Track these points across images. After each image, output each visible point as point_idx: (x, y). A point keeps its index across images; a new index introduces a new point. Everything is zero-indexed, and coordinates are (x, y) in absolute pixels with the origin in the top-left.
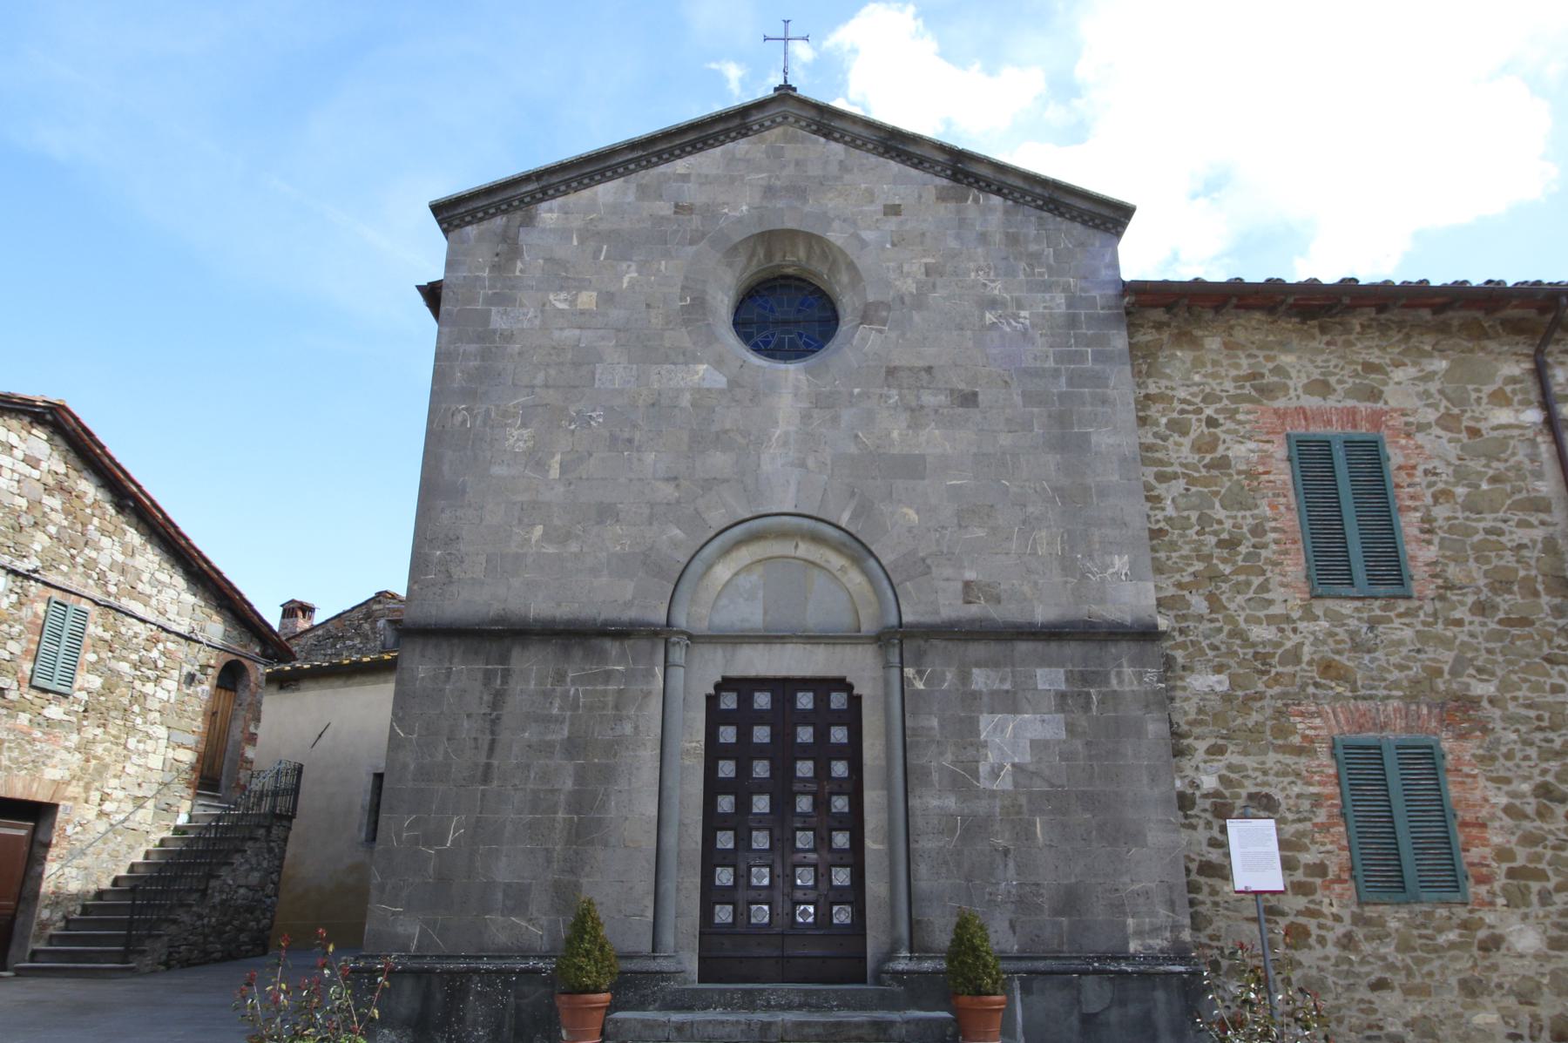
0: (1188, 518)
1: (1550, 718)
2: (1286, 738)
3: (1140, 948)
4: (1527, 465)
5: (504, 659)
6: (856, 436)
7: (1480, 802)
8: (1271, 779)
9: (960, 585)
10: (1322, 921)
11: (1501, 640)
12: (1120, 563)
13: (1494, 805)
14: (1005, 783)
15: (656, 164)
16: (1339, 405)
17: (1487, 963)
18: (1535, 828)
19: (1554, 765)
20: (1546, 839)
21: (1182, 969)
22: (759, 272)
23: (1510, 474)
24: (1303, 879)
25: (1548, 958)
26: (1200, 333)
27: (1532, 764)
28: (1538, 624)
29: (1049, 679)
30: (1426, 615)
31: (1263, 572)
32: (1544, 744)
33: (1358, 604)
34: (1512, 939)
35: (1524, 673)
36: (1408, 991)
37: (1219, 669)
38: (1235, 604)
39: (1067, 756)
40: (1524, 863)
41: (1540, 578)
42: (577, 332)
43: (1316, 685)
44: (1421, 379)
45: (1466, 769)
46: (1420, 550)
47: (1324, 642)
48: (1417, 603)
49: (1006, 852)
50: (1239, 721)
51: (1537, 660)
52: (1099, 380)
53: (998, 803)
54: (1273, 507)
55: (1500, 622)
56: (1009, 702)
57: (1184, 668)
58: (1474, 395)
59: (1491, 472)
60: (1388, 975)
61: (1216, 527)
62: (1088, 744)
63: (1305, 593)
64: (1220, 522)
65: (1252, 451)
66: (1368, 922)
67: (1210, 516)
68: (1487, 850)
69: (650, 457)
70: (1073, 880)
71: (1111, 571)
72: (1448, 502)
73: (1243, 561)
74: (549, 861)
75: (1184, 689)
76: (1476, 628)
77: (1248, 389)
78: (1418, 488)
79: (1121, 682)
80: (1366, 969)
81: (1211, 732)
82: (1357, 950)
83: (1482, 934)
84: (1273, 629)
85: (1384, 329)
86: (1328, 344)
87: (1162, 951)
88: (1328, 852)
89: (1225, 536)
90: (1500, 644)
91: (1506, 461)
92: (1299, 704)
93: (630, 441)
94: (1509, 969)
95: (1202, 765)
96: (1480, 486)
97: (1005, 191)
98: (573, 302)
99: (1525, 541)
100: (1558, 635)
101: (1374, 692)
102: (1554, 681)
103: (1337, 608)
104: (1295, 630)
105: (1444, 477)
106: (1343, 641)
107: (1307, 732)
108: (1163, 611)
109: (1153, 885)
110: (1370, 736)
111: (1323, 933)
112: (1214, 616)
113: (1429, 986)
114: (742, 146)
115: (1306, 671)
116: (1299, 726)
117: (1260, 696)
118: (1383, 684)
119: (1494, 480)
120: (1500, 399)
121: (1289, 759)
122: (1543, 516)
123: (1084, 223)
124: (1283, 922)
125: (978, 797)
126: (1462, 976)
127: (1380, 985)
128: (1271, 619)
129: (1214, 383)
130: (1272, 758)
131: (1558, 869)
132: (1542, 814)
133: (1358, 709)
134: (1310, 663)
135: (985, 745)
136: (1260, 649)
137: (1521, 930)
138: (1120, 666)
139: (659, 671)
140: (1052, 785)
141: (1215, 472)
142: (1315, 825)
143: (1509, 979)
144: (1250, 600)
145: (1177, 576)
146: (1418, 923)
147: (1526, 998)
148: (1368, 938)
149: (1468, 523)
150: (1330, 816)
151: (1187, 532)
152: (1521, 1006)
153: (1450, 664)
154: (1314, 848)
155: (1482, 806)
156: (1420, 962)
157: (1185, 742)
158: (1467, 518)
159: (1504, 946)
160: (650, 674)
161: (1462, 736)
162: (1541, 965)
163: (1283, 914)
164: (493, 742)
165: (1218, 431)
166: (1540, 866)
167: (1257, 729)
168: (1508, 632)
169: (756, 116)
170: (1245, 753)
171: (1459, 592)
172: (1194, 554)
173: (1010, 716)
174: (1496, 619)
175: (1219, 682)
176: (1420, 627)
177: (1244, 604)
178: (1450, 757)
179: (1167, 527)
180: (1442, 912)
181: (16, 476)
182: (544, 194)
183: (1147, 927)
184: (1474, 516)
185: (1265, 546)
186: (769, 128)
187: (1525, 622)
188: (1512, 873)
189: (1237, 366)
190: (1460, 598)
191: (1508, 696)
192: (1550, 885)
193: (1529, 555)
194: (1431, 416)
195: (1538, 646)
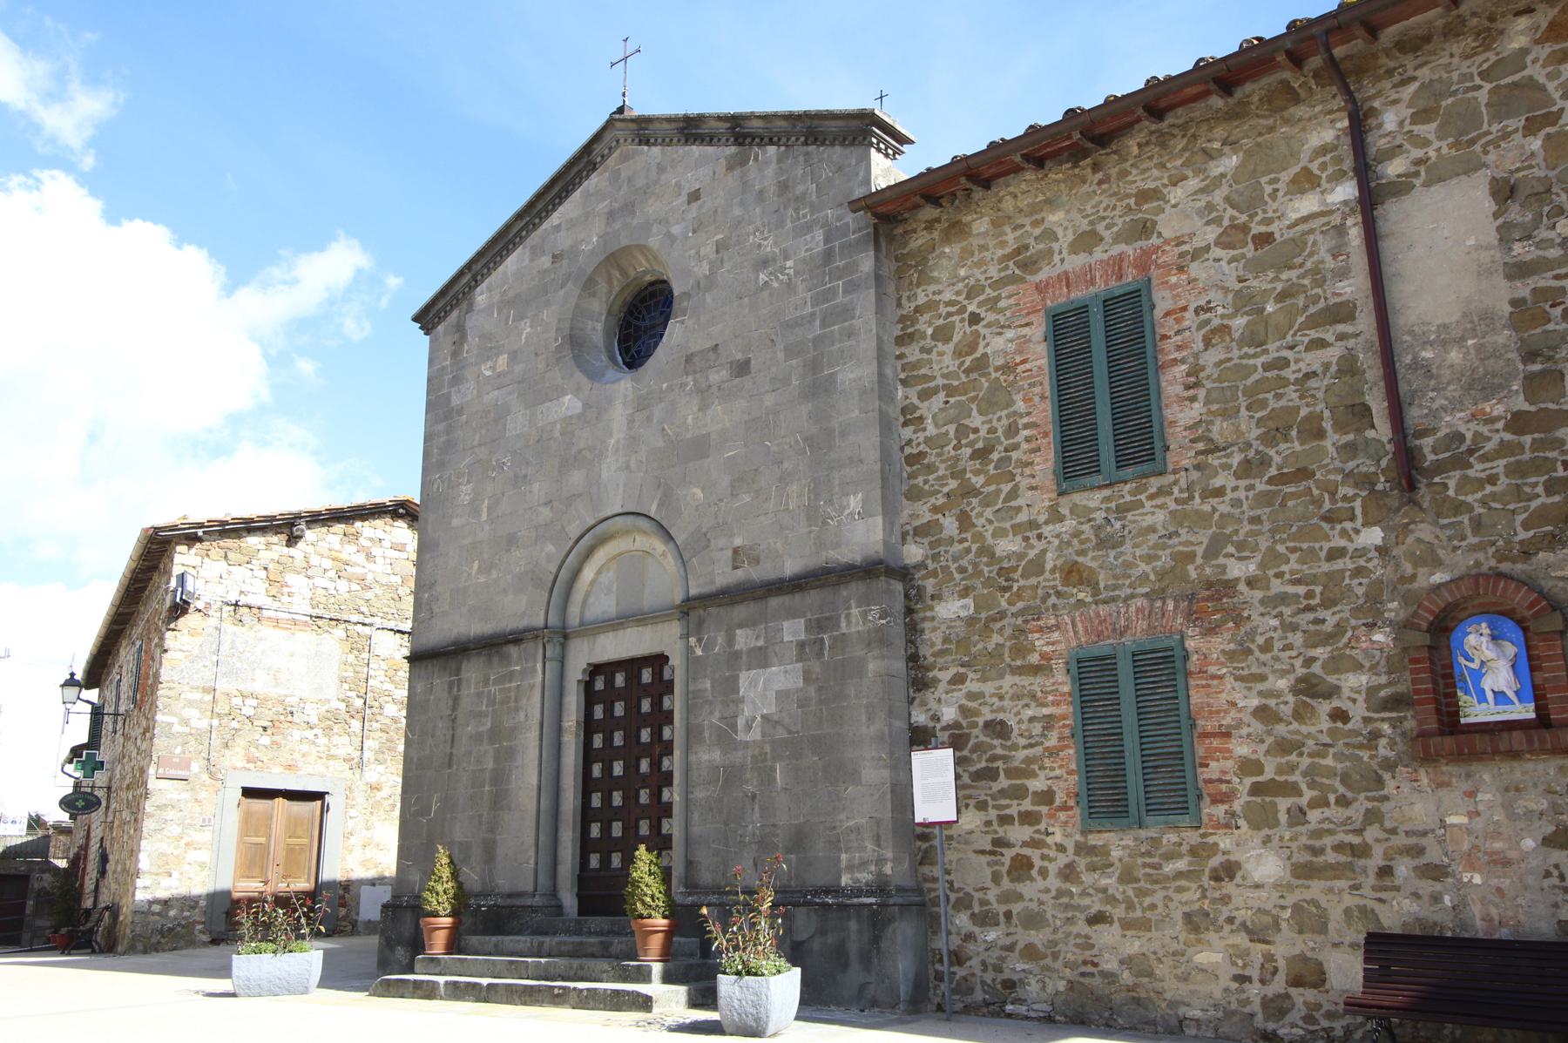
0: (947, 433)
1: (1322, 594)
2: (1024, 658)
3: (850, 882)
4: (1330, 263)
5: (458, 671)
6: (663, 429)
7: (1225, 707)
8: (1007, 703)
9: (729, 553)
10: (1046, 851)
11: (1270, 504)
12: (854, 502)
13: (1240, 710)
14: (755, 735)
15: (540, 224)
16: (1105, 256)
17: (1217, 895)
18: (1289, 732)
19: (1321, 652)
20: (1304, 745)
21: (873, 900)
22: (622, 290)
23: (1306, 282)
24: (1030, 808)
25: (1290, 888)
26: (969, 218)
27: (1294, 653)
28: (1318, 476)
29: (793, 630)
30: (1181, 491)
31: (1012, 477)
32: (1312, 627)
33: (1107, 492)
34: (1249, 866)
35: (1294, 541)
36: (1127, 925)
37: (964, 593)
38: (983, 518)
39: (802, 704)
40: (1272, 776)
41: (1327, 414)
42: (496, 392)
43: (1059, 594)
44: (1202, 191)
45: (1212, 670)
46: (1181, 411)
47: (1069, 544)
48: (1171, 478)
49: (754, 797)
50: (980, 646)
51: (1315, 521)
52: (846, 313)
53: (750, 752)
54: (1027, 400)
55: (1271, 481)
56: (760, 658)
57: (933, 597)
58: (1268, 189)
59: (1279, 286)
60: (1108, 908)
61: (972, 436)
62: (820, 689)
63: (1052, 491)
64: (976, 431)
65: (1011, 341)
66: (1091, 850)
67: (967, 426)
68: (1229, 764)
69: (536, 486)
70: (802, 820)
71: (847, 512)
72: (1223, 341)
73: (995, 468)
74: (480, 823)
75: (933, 619)
76: (1241, 494)
77: (1013, 268)
78: (1187, 333)
79: (849, 623)
80: (1086, 901)
81: (954, 661)
82: (1079, 882)
83: (1215, 861)
84: (1019, 538)
85: (1163, 140)
86: (1100, 183)
87: (867, 884)
88: (1056, 778)
89: (980, 445)
90: (1267, 510)
91: (1301, 266)
92: (1038, 619)
93: (525, 476)
94: (1243, 902)
95: (944, 696)
96: (1264, 309)
97: (775, 139)
98: (493, 368)
99: (1316, 367)
100: (1343, 484)
101: (1117, 593)
102: (1332, 544)
103: (1085, 502)
104: (1039, 537)
105: (1220, 310)
106: (1088, 540)
107: (1045, 648)
108: (918, 539)
109: (864, 821)
110: (1105, 646)
111: (1046, 864)
112: (963, 536)
113: (1150, 920)
114: (594, 182)
115: (1049, 581)
116: (1037, 643)
117: (1002, 615)
118: (1127, 582)
119: (1282, 296)
120: (1306, 182)
121: (1024, 681)
122: (1341, 328)
123: (842, 144)
124: (1009, 853)
125: (735, 749)
126: (1187, 909)
127: (1098, 919)
128: (1016, 529)
129: (977, 272)
130: (1009, 680)
131: (1313, 781)
132: (1298, 715)
133: (1098, 615)
134: (1053, 571)
135: (742, 700)
136: (1005, 565)
137: (1260, 855)
138: (849, 608)
139: (539, 666)
140: (790, 732)
141: (974, 375)
142: (1047, 749)
143: (1243, 912)
144: (999, 510)
145: (933, 500)
146: (1143, 850)
147: (1257, 934)
148: (1092, 868)
149: (1244, 362)
150: (1061, 739)
151: (946, 449)
152: (1251, 945)
153: (1204, 546)
154: (1042, 774)
155: (1226, 712)
156: (1142, 893)
157: (931, 674)
158: (1246, 356)
159: (1239, 875)
160: (534, 670)
161: (1211, 631)
162: (1282, 897)
163: (1008, 845)
164: (453, 736)
165: (979, 327)
166: (1292, 778)
167: (996, 654)
168: (1280, 491)
169: (598, 148)
170: (984, 680)
171: (1223, 453)
172: (948, 472)
173: (761, 671)
174: (1266, 478)
175: (963, 607)
176: (1173, 506)
177: (991, 517)
178: (1194, 658)
179: (928, 450)
180: (1173, 837)
181: (388, 561)
182: (476, 282)
183: (857, 862)
184: (1251, 351)
185: (1016, 447)
186: (610, 154)
187: (1304, 473)
188: (1256, 789)
189: (1003, 244)
190: (1224, 460)
191: (1271, 573)
192: (1304, 801)
193: (1316, 385)
194: (1211, 234)
195: (1318, 503)
